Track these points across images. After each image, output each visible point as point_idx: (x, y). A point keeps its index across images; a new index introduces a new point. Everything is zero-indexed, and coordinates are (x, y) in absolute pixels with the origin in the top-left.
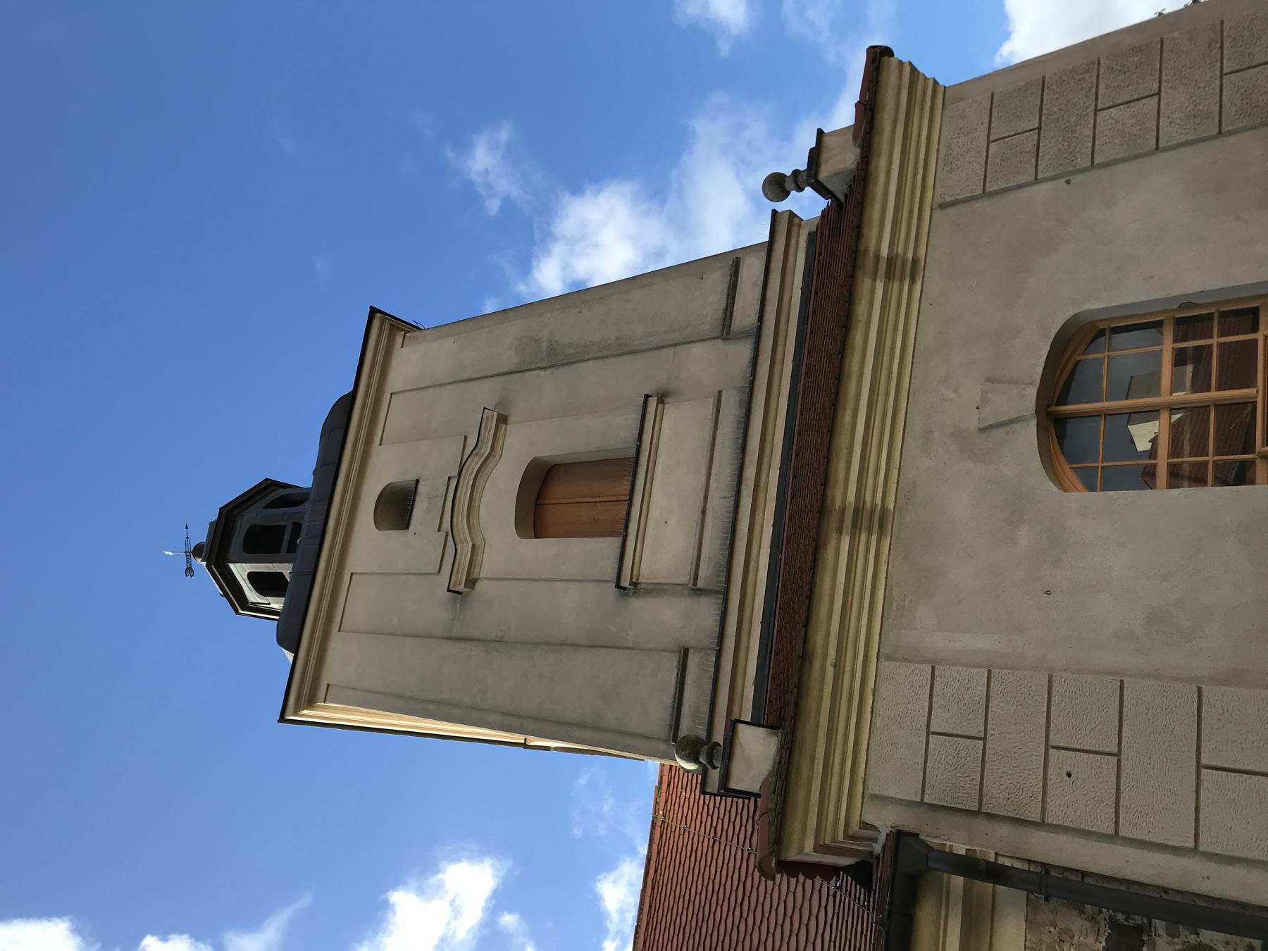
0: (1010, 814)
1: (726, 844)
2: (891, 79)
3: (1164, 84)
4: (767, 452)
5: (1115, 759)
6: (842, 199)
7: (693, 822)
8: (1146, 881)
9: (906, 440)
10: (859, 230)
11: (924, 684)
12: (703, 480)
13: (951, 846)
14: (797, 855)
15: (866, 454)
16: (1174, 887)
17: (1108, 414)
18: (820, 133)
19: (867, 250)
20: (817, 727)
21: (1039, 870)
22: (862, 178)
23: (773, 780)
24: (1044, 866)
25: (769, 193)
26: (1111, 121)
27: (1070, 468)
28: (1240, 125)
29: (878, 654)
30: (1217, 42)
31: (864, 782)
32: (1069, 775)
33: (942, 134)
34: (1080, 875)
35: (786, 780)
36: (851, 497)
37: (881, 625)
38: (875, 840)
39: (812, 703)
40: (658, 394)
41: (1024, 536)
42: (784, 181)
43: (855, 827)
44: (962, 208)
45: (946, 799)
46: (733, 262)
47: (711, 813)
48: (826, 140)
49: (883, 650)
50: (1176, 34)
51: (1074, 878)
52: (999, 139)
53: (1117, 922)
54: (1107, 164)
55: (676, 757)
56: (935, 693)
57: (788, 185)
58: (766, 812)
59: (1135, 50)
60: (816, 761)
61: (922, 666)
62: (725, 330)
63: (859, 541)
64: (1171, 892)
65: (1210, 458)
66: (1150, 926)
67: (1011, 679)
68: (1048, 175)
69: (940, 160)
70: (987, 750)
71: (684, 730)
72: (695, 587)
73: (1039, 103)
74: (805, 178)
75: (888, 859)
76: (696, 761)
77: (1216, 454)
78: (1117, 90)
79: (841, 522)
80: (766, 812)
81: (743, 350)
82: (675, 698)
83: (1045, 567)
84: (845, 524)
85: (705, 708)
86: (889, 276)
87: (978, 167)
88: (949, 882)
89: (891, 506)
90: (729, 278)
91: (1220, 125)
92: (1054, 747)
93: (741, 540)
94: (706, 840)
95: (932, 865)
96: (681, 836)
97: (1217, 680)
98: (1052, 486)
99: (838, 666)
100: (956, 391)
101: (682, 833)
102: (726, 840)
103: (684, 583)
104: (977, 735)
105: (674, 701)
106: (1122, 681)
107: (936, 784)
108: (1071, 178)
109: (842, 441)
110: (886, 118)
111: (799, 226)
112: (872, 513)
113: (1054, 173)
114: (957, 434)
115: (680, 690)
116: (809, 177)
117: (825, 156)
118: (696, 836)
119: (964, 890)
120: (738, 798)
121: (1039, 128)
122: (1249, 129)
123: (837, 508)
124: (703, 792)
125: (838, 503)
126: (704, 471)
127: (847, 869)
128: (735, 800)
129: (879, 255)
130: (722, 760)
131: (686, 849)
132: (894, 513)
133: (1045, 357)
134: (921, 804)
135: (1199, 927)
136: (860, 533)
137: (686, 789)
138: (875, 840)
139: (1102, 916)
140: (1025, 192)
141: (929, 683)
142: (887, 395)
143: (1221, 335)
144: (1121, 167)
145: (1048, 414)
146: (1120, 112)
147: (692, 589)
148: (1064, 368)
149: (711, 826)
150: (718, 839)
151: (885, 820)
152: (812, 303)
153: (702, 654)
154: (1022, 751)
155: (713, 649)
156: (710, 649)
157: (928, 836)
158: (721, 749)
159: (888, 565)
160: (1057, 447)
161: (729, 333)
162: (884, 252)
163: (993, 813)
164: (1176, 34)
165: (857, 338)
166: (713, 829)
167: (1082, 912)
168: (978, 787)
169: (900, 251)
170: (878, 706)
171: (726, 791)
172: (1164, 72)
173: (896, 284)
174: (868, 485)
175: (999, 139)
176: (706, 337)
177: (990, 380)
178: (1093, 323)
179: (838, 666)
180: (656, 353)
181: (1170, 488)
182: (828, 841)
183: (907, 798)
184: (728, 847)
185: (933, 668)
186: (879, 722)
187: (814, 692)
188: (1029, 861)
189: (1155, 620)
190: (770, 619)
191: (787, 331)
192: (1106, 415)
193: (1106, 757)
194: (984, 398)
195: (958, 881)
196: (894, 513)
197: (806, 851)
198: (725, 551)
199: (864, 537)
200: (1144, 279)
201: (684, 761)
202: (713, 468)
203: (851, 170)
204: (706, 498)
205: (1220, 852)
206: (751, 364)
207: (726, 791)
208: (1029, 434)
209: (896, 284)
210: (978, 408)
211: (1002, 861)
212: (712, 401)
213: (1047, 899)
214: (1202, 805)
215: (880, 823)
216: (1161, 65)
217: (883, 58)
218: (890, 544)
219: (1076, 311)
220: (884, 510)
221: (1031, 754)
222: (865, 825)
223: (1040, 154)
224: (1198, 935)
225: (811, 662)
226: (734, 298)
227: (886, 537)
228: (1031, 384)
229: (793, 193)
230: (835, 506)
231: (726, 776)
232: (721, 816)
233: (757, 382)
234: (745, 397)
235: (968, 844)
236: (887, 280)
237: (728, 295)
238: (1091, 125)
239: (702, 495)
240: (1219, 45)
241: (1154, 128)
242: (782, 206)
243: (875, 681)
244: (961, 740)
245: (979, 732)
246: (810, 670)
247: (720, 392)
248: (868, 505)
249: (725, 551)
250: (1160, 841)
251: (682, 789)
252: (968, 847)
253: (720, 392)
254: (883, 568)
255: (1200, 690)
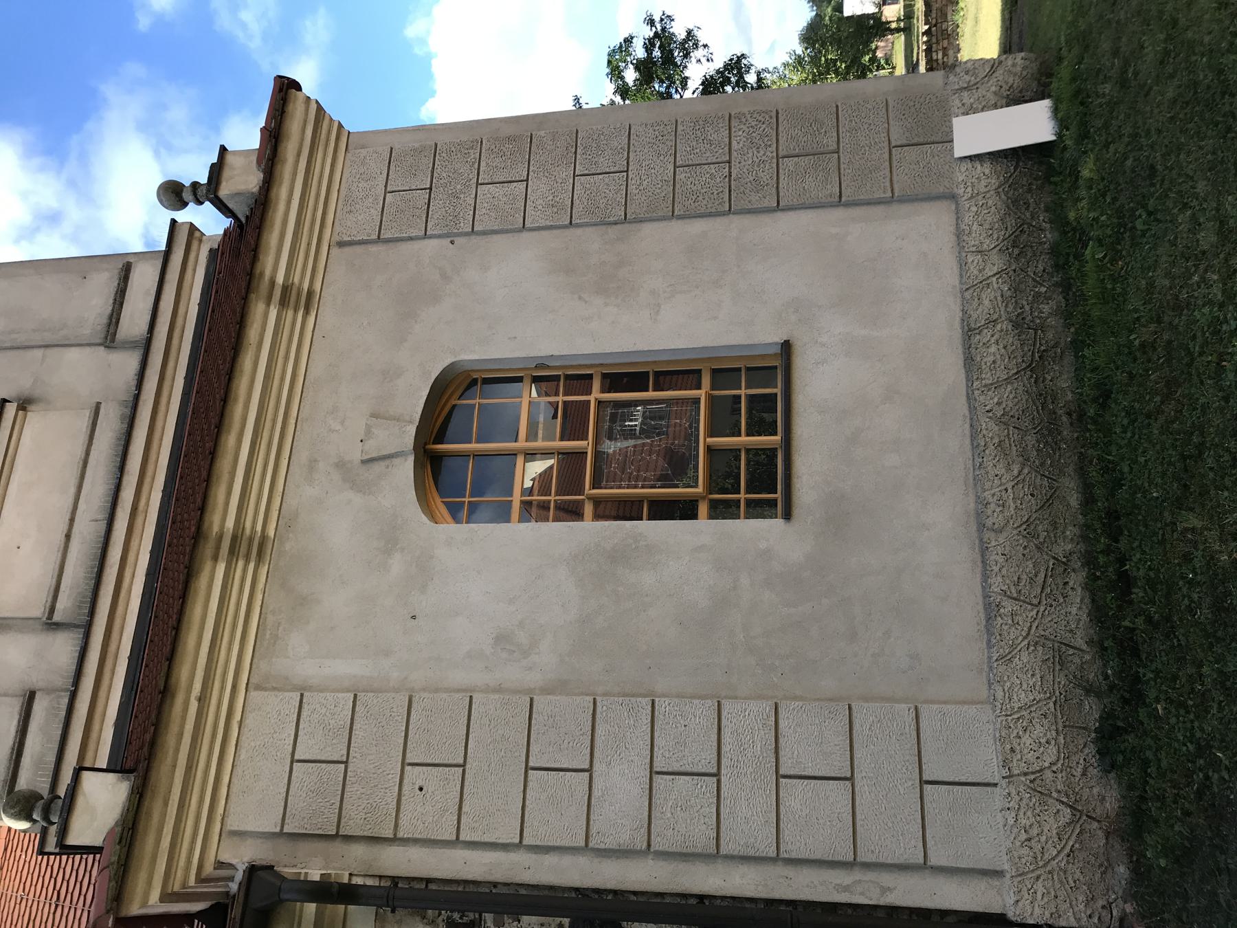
0: (366, 834)
1: (83, 910)
2: (296, 112)
3: (531, 173)
4: (149, 473)
5: (715, 779)
6: (243, 220)
7: (33, 888)
8: (479, 879)
9: (291, 468)
10: (255, 252)
11: (292, 711)
12: (71, 500)
13: (306, 873)
14: (140, 908)
15: (248, 479)
16: (501, 881)
17: (478, 455)
18: (223, 149)
19: (262, 274)
20: (174, 766)
21: (388, 884)
22: (262, 202)
23: (119, 829)
24: (395, 880)
25: (164, 199)
26: (489, 195)
27: (443, 502)
28: (586, 220)
29: (247, 684)
30: (572, 147)
31: (223, 819)
32: (421, 789)
33: (344, 176)
34: (425, 883)
35: (133, 828)
36: (230, 524)
37: (253, 656)
38: (231, 879)
39: (170, 740)
40: (20, 400)
41: (397, 565)
42: (182, 191)
43: (209, 869)
44: (358, 249)
45: (306, 826)
46: (125, 267)
47: (54, 875)
48: (229, 159)
49: (253, 681)
50: (542, 133)
51: (417, 886)
52: (395, 191)
53: (453, 921)
54: (484, 233)
55: (3, 816)
56: (301, 720)
57: (187, 195)
58: (108, 867)
59: (510, 139)
60: (170, 802)
61: (291, 694)
62: (110, 337)
63: (235, 569)
64: (499, 886)
65: (742, 496)
66: (481, 920)
67: (375, 701)
68: (435, 232)
69: (340, 202)
70: (349, 773)
71: (23, 783)
72: (50, 621)
73: (431, 165)
74: (205, 192)
75: (241, 899)
76: (28, 818)
77: (557, 494)
78: (495, 170)
79: (218, 548)
80: (108, 867)
81: (131, 361)
82: (13, 749)
83: (413, 593)
84: (221, 550)
85: (51, 758)
86: (284, 303)
87: (376, 213)
88: (301, 910)
89: (271, 533)
90: (117, 282)
91: (571, 217)
92: (410, 764)
93: (111, 567)
94: (47, 905)
95: (284, 896)
96: (18, 906)
97: (547, 690)
98: (424, 519)
99: (203, 699)
100: (342, 423)
101: (18, 902)
102: (71, 903)
103: (34, 616)
104: (340, 759)
105: (12, 753)
106: (471, 696)
107: (297, 813)
108: (455, 239)
109: (224, 464)
110: (290, 148)
111: (200, 241)
112: (251, 540)
113: (440, 232)
114: (341, 465)
115: (20, 740)
116: (209, 191)
117: (226, 173)
118: (35, 904)
119: (316, 914)
120: (88, 854)
121: (431, 189)
122: (591, 225)
123: (214, 534)
124: (41, 852)
125: (216, 529)
126: (73, 490)
127: (200, 915)
128: (85, 856)
129: (274, 282)
130: (61, 813)
131: (23, 920)
132: (274, 541)
133: (425, 398)
134: (281, 834)
135: (521, 915)
136: (237, 560)
137: (26, 851)
138: (231, 879)
139: (441, 918)
140: (417, 245)
141: (297, 710)
142: (274, 421)
143: (565, 394)
144: (495, 237)
145: (425, 451)
146: (497, 190)
147: (47, 624)
148: (442, 409)
149: (54, 889)
150: (61, 903)
151: (241, 856)
152: (208, 321)
153: (53, 696)
154: (381, 770)
155: (66, 690)
156: (62, 690)
157: (285, 866)
158: (60, 802)
159: (264, 593)
160: (431, 479)
161: (113, 340)
162: (280, 279)
163: (351, 834)
164: (542, 133)
165: (246, 362)
166: (56, 892)
167: (424, 918)
168: (337, 811)
169: (296, 280)
170: (243, 738)
171: (66, 850)
172: (531, 164)
173: (290, 313)
174: (249, 511)
175: (395, 191)
176: (85, 342)
177: (375, 415)
178: (467, 373)
179: (203, 699)
180: (21, 352)
181: (747, 518)
182: (177, 888)
183: (266, 830)
184: (72, 911)
185: (302, 695)
186: (243, 755)
187: (174, 728)
188: (381, 877)
189: (502, 639)
190: (139, 654)
191: (180, 346)
192: (474, 456)
193: (453, 769)
194: (368, 431)
195: (311, 908)
196: (274, 541)
197: (150, 903)
198: (92, 579)
199: (241, 564)
200: (509, 338)
201: (13, 821)
202: (84, 487)
203: (253, 193)
204: (72, 520)
205: (539, 843)
206: (137, 377)
207: (66, 850)
208: (406, 468)
209: (290, 313)
210: (362, 441)
211: (358, 881)
212: (88, 415)
213: (393, 911)
214: (527, 802)
215: (237, 860)
216: (529, 157)
217: (290, 91)
218: (268, 572)
219: (454, 360)
220: (264, 537)
221: (388, 772)
222: (220, 865)
223: (430, 213)
224: (519, 921)
225: (173, 696)
226: (121, 304)
227: (264, 565)
228: (411, 422)
229: (191, 205)
230: (212, 532)
231: (63, 831)
232: (67, 877)
233: (143, 397)
234: (128, 411)
235: (324, 868)
236: (281, 307)
237: (115, 300)
238: (473, 196)
239: (68, 517)
240: (574, 150)
241: (522, 208)
242: (183, 216)
243: (243, 712)
244: (324, 765)
245: (342, 756)
246: (172, 705)
247: (98, 404)
248: (248, 532)
249: (92, 579)
250: (492, 840)
251: (22, 851)
252: (323, 872)
253: (98, 404)
254: (259, 597)
255: (532, 700)
